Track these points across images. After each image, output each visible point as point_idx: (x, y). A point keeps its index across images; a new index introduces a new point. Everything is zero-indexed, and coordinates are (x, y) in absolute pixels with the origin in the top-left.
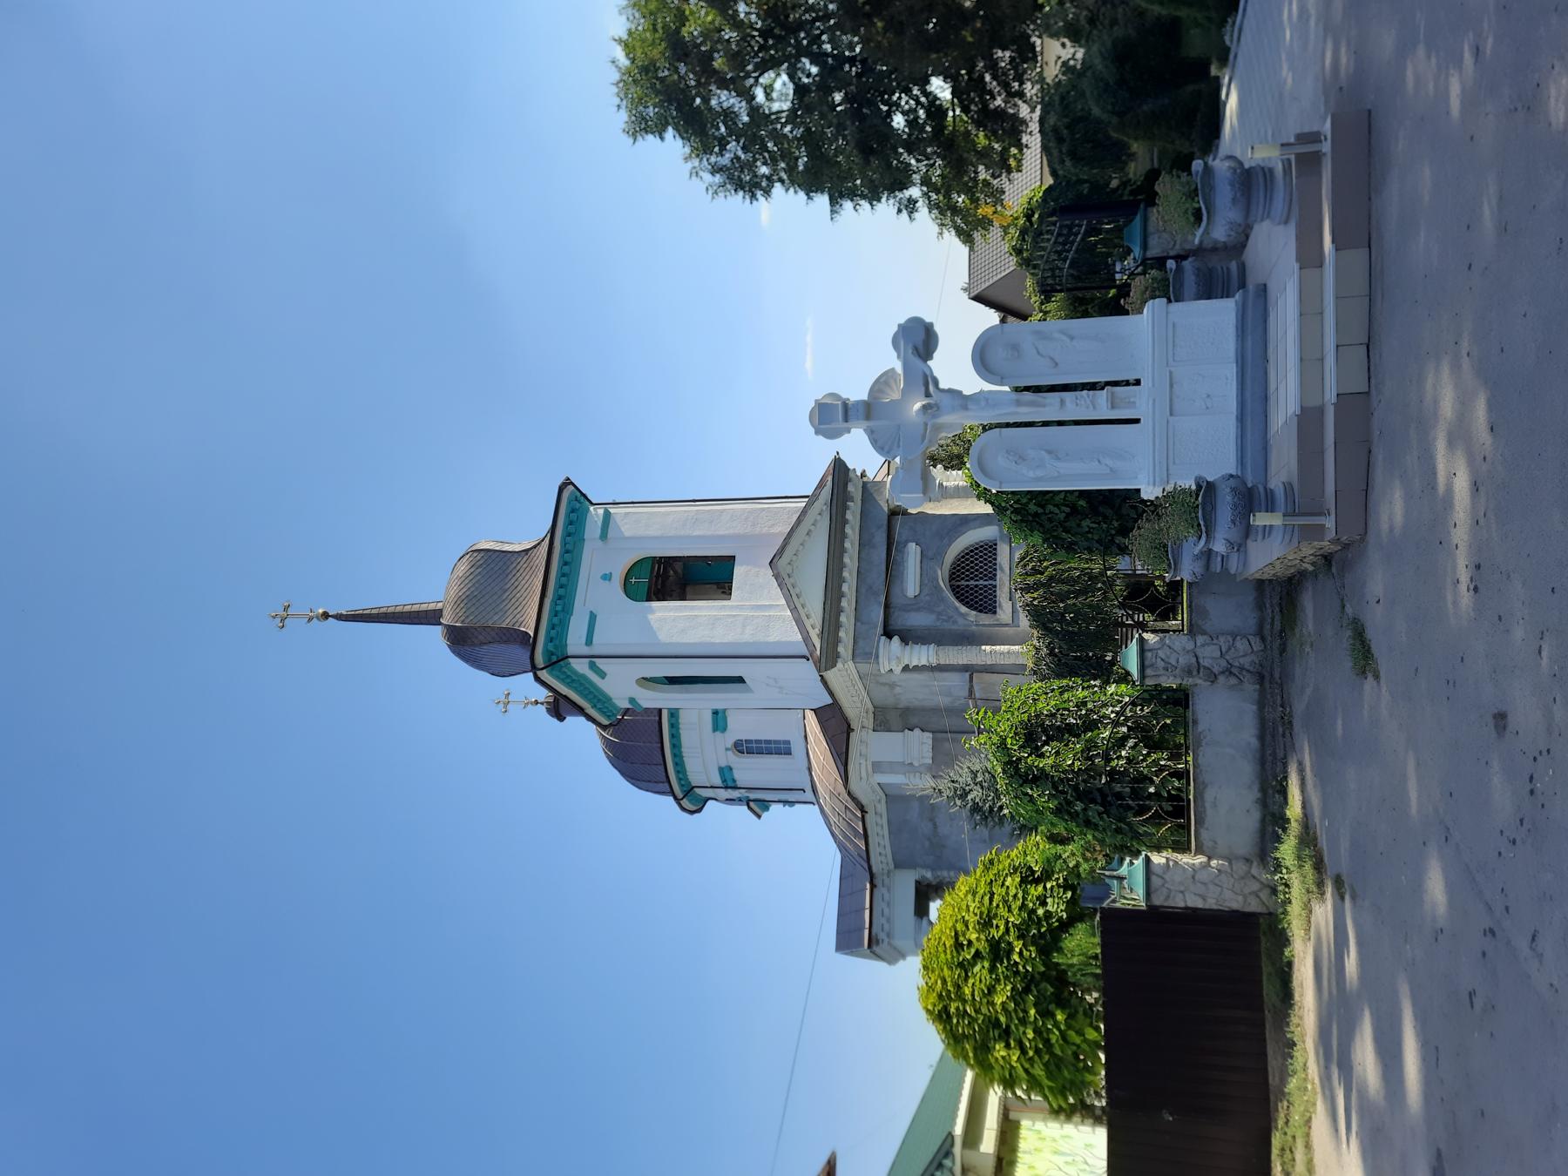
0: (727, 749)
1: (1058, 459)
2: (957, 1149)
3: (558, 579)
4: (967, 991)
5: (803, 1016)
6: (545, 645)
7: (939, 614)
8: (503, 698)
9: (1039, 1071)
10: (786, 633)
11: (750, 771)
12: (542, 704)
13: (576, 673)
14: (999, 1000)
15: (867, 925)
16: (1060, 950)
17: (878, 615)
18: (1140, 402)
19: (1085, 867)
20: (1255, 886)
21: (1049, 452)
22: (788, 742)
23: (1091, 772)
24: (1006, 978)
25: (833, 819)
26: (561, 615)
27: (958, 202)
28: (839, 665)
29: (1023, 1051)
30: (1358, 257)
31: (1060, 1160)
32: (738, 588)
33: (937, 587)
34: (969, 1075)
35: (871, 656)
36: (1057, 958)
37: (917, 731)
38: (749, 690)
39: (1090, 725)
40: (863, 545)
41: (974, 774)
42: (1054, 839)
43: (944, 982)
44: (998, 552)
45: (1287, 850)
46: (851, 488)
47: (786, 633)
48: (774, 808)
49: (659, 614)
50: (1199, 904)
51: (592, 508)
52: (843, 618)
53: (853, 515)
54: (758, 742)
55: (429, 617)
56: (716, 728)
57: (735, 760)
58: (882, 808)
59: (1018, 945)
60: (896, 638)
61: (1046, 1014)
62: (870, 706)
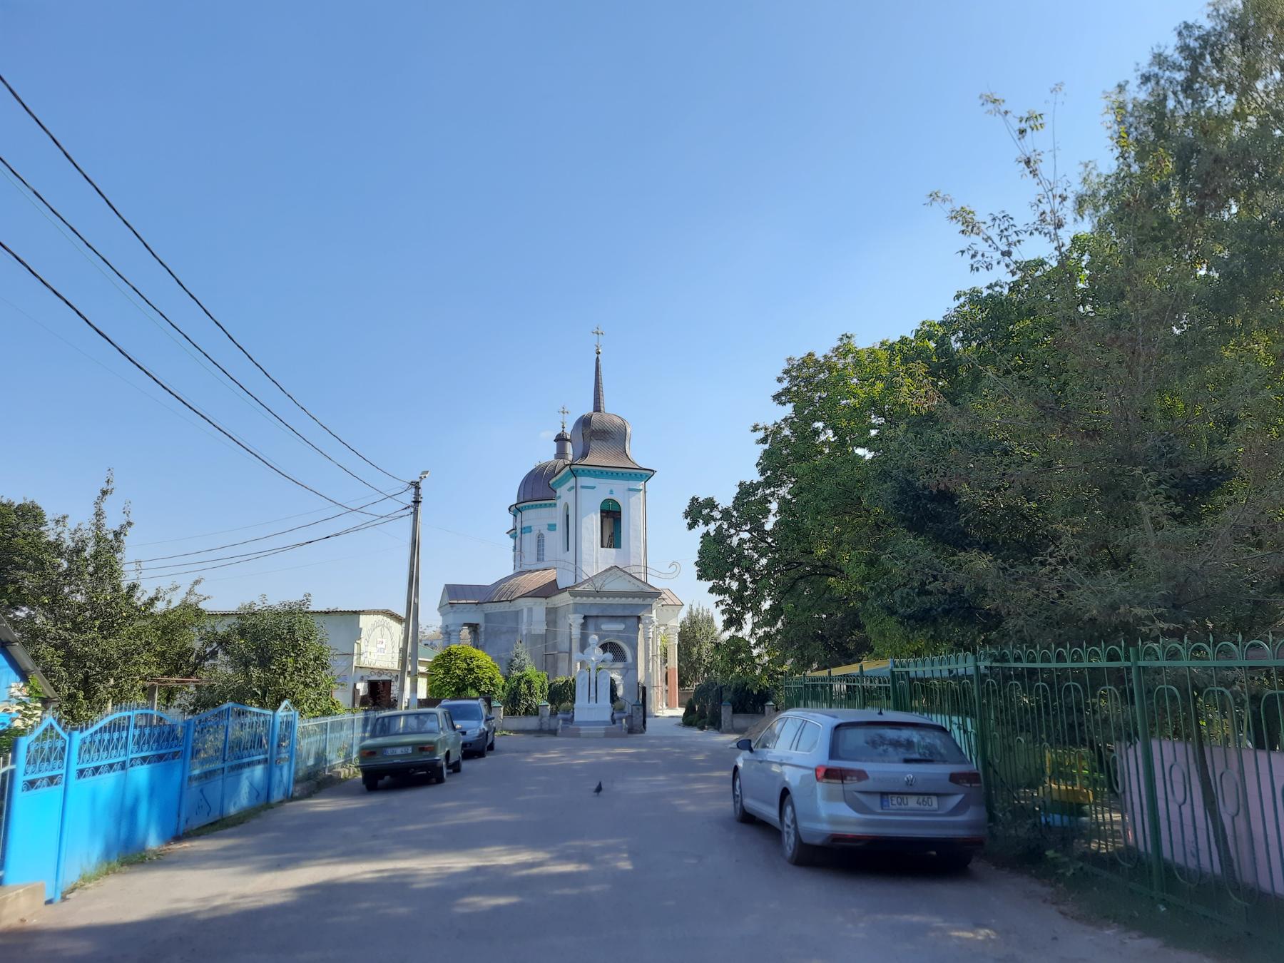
0: (540, 531)
5: (247, 354)
8: (566, 410)
9: (437, 683)
11: (529, 541)
12: (563, 431)
14: (457, 671)
15: (459, 602)
17: (594, 613)
19: (496, 696)
23: (521, 696)
27: (249, 732)
28: (571, 598)
34: (431, 660)
35: (576, 612)
36: (469, 688)
37: (545, 627)
38: (564, 552)
39: (531, 695)
41: (524, 660)
42: (504, 687)
46: (649, 599)
48: (512, 541)
49: (594, 517)
53: (637, 601)
54: (543, 545)
55: (597, 408)
56: (549, 525)
57: (535, 533)
58: (512, 609)
59: (473, 677)
60: (583, 621)
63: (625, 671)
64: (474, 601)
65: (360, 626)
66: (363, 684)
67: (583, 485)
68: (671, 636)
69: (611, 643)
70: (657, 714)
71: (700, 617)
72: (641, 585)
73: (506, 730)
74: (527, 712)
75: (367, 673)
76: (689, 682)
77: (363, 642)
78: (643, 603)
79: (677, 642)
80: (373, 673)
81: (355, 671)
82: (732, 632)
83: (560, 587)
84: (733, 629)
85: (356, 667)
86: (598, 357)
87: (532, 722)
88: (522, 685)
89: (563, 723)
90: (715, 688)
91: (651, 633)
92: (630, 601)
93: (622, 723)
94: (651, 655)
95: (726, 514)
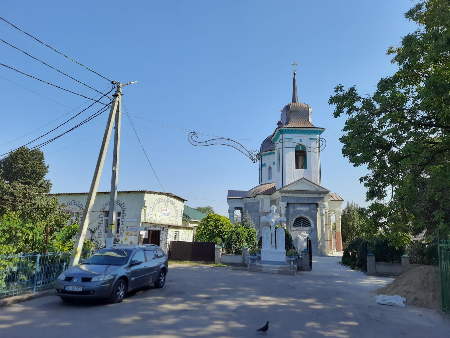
1: (266, 238)
2: (189, 220)
3: (300, 130)
4: (211, 222)
6: (284, 129)
7: (293, 215)
9: (200, 233)
10: (288, 181)
11: (265, 170)
13: (279, 136)
14: (210, 227)
15: (233, 198)
16: (217, 237)
17: (292, 201)
18: (274, 249)
20: (218, 261)
21: (267, 237)
22: (271, 179)
23: (232, 242)
24: (213, 228)
25: (251, 191)
26: (292, 132)
28: (280, 194)
29: (203, 231)
30: (277, 272)
31: (188, 236)
32: (298, 170)
33: (299, 214)
34: (200, 221)
39: (239, 242)
40: (309, 198)
43: (213, 218)
44: (308, 227)
45: (221, 264)
47: (288, 181)
50: (215, 254)
51: (318, 135)
52: (291, 194)
53: (315, 196)
55: (294, 100)
58: (256, 201)
60: (287, 205)
61: (208, 234)
62: (275, 199)
63: (311, 231)
64: (239, 198)
65: (145, 200)
66: (145, 232)
67: (286, 137)
68: (337, 216)
69: (302, 217)
70: (329, 255)
71: (353, 208)
72: (318, 188)
73: (222, 263)
74: (236, 253)
75: (149, 226)
76: (348, 239)
77: (148, 209)
78: (319, 197)
79: (341, 219)
80: (151, 226)
81: (142, 225)
82: (374, 201)
83: (276, 189)
84: (375, 199)
85: (143, 222)
86: (294, 76)
87: (238, 259)
88: (234, 236)
89: (251, 262)
90: (362, 243)
91: (324, 213)
92: (312, 195)
93: (291, 264)
94: (324, 224)
95: (367, 104)
